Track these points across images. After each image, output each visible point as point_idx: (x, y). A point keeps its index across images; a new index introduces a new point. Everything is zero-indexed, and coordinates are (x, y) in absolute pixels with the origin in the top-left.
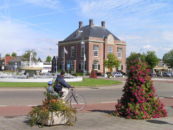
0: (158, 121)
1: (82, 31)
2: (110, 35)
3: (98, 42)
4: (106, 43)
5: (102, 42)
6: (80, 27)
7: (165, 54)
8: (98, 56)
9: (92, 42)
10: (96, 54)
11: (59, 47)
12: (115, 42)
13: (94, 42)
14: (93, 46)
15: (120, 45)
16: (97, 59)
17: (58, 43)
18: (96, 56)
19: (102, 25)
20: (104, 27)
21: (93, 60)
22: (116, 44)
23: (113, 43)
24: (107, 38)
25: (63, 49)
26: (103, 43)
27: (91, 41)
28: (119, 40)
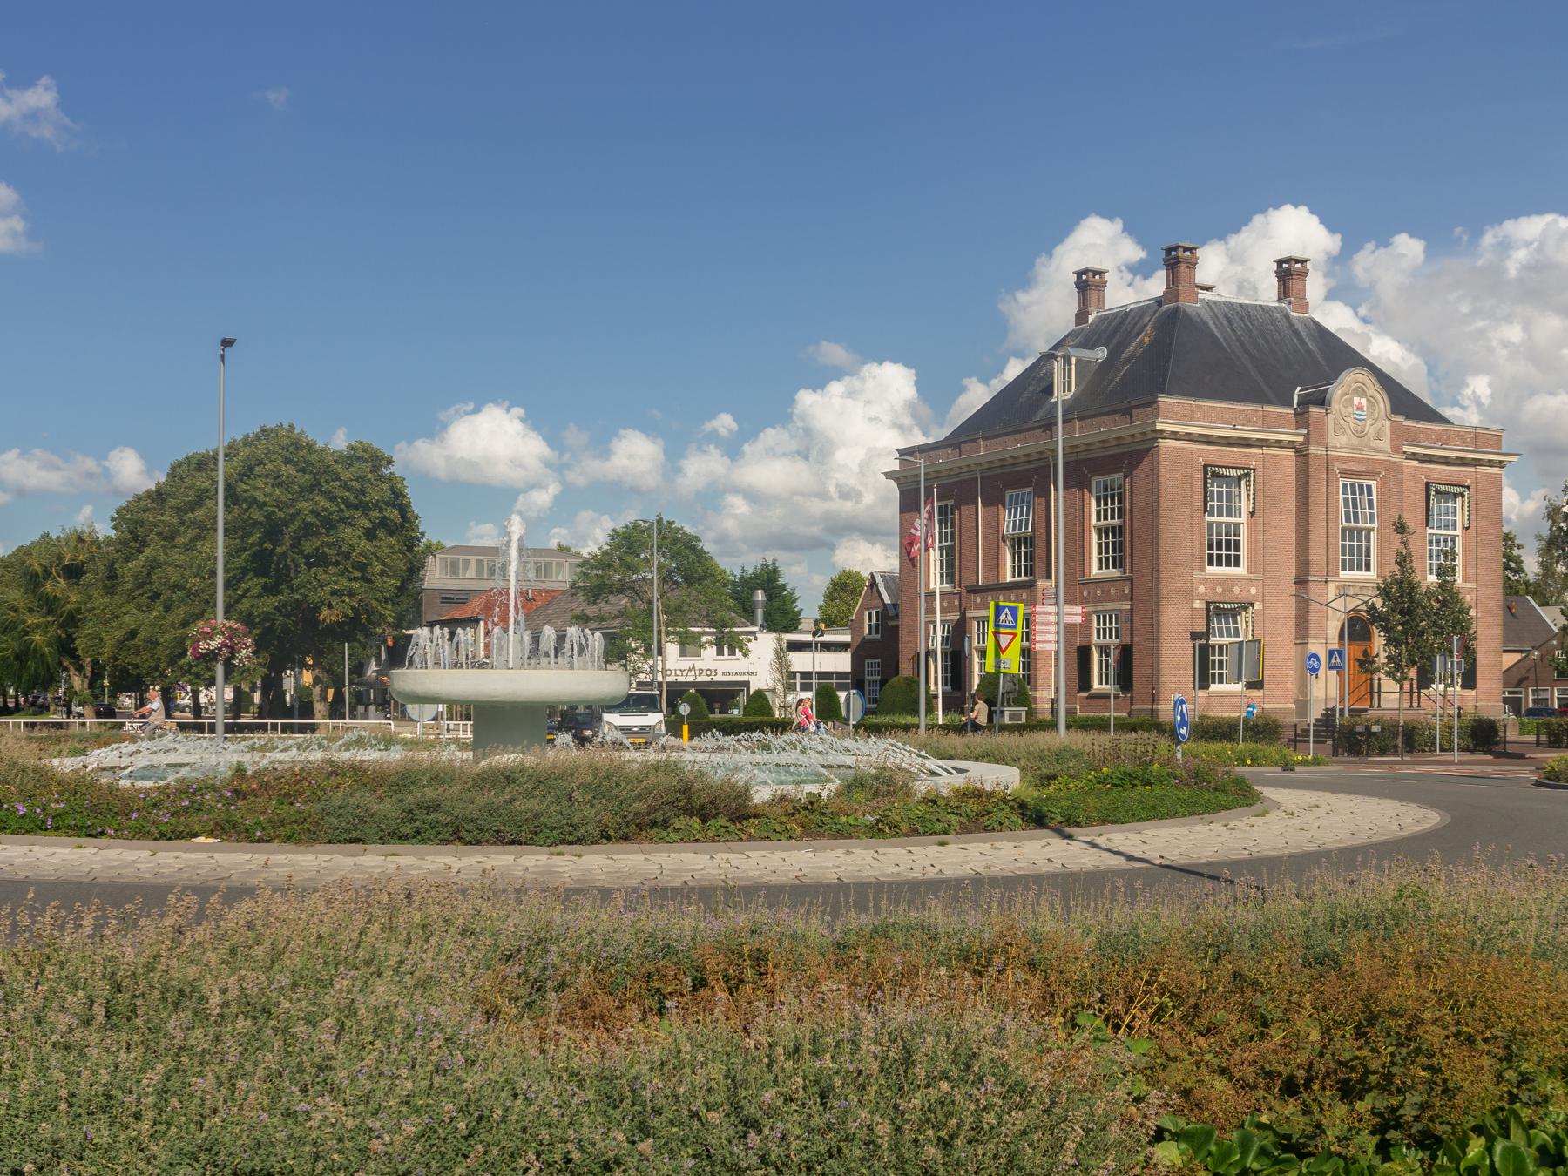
0: (1347, 792)
1: (1101, 353)
2: (1352, 377)
3: (1246, 443)
4: (1315, 450)
5: (1279, 444)
6: (1081, 316)
7: (271, 425)
8: (1241, 571)
9: (1189, 437)
10: (1223, 550)
11: (901, 493)
12: (1399, 437)
13: (1207, 440)
14: (1199, 475)
15: (1446, 461)
16: (1236, 590)
17: (895, 466)
18: (1223, 570)
19: (1284, 293)
20: (1305, 307)
21: (1199, 605)
22: (1413, 456)
23: (1385, 444)
24: (1322, 401)
25: (977, 690)
26: (1291, 445)
27: (1175, 436)
28: (1444, 420)
